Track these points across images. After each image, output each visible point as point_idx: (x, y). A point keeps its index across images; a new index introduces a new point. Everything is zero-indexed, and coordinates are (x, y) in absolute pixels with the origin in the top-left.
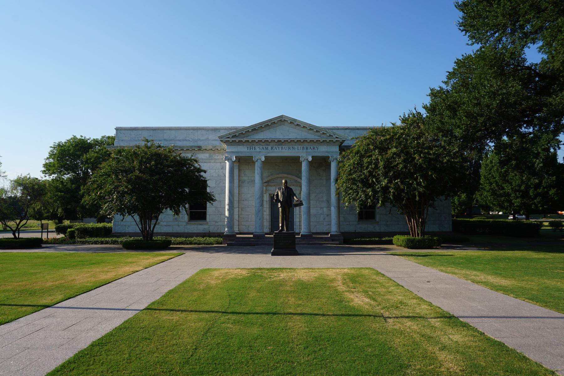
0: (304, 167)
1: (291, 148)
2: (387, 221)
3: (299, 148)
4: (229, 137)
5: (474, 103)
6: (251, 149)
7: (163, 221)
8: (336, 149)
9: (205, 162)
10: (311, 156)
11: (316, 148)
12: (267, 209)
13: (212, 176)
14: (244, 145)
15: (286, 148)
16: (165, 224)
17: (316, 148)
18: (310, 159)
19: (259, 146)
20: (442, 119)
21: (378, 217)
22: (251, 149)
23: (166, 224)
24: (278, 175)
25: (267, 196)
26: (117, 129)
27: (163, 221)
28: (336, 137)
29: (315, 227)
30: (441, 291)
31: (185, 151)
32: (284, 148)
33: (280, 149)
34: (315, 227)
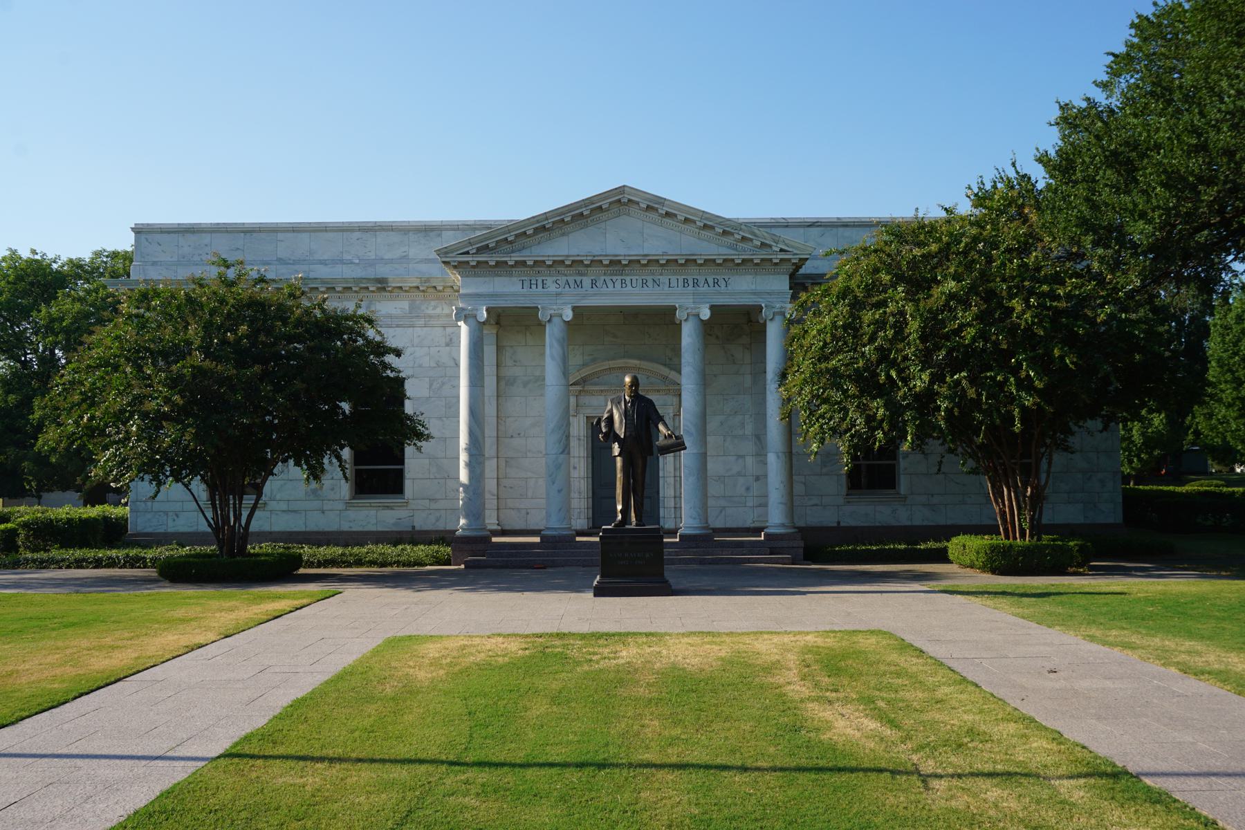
0: (689, 336)
1: (650, 283)
2: (932, 495)
3: (674, 283)
4: (467, 253)
6: (534, 286)
8: (781, 284)
9: (398, 326)
11: (722, 283)
12: (582, 459)
13: (420, 366)
14: (511, 275)
15: (634, 281)
16: (284, 506)
17: (722, 283)
19: (555, 278)
21: (904, 484)
22: (534, 286)
25: (582, 424)
28: (782, 250)
29: (721, 512)
32: (628, 283)
33: (618, 284)
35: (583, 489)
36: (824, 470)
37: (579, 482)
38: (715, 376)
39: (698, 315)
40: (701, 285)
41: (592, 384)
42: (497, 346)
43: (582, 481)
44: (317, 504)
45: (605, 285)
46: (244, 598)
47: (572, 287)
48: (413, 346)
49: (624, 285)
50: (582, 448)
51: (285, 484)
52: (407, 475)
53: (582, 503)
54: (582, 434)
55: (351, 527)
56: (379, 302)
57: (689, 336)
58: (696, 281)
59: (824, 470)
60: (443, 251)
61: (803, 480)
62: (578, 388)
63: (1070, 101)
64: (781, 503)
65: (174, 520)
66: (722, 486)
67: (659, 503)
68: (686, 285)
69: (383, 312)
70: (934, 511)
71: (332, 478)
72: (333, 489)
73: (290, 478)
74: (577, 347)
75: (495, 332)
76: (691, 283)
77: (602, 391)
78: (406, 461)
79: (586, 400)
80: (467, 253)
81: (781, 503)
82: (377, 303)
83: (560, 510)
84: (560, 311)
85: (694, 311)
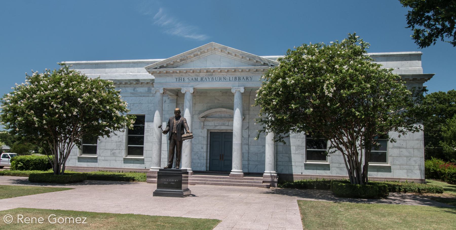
0: (237, 100)
2: (341, 164)
4: (156, 68)
5: (382, 82)
7: (102, 155)
9: (144, 96)
10: (243, 87)
12: (205, 145)
13: (150, 110)
15: (216, 78)
16: (103, 158)
18: (242, 90)
19: (188, 77)
20: (360, 105)
22: (180, 80)
23: (103, 159)
24: (216, 109)
25: (205, 132)
26: (439, 92)
27: (102, 155)
29: (256, 167)
30: (381, 112)
31: (124, 84)
32: (214, 79)
34: (256, 167)
35: (205, 156)
36: (297, 152)
37: (204, 153)
38: (255, 115)
39: (239, 91)
40: (241, 80)
41: (209, 118)
42: (177, 103)
43: (205, 153)
44: (114, 158)
45: (206, 80)
46: (445, 151)
47: (194, 80)
48: (148, 103)
49: (213, 80)
50: (205, 141)
51: (104, 151)
52: (144, 149)
53: (204, 161)
54: (205, 136)
55: (125, 167)
56: (138, 87)
57: (237, 100)
58: (239, 78)
59: (297, 152)
60: (147, 68)
61: (288, 156)
62: (204, 119)
63: (409, 11)
64: (269, 164)
65: (68, 162)
66: (257, 157)
67: (74, 174)
68: (236, 79)
69: (139, 91)
70: (341, 170)
71: (119, 149)
72: (119, 153)
73: (106, 149)
74: (205, 104)
75: (176, 98)
76: (238, 79)
77: (213, 120)
78: (144, 144)
79: (206, 123)
80: (156, 68)
81: (269, 164)
82: (137, 88)
83: (186, 163)
84: (189, 90)
85: (238, 90)
